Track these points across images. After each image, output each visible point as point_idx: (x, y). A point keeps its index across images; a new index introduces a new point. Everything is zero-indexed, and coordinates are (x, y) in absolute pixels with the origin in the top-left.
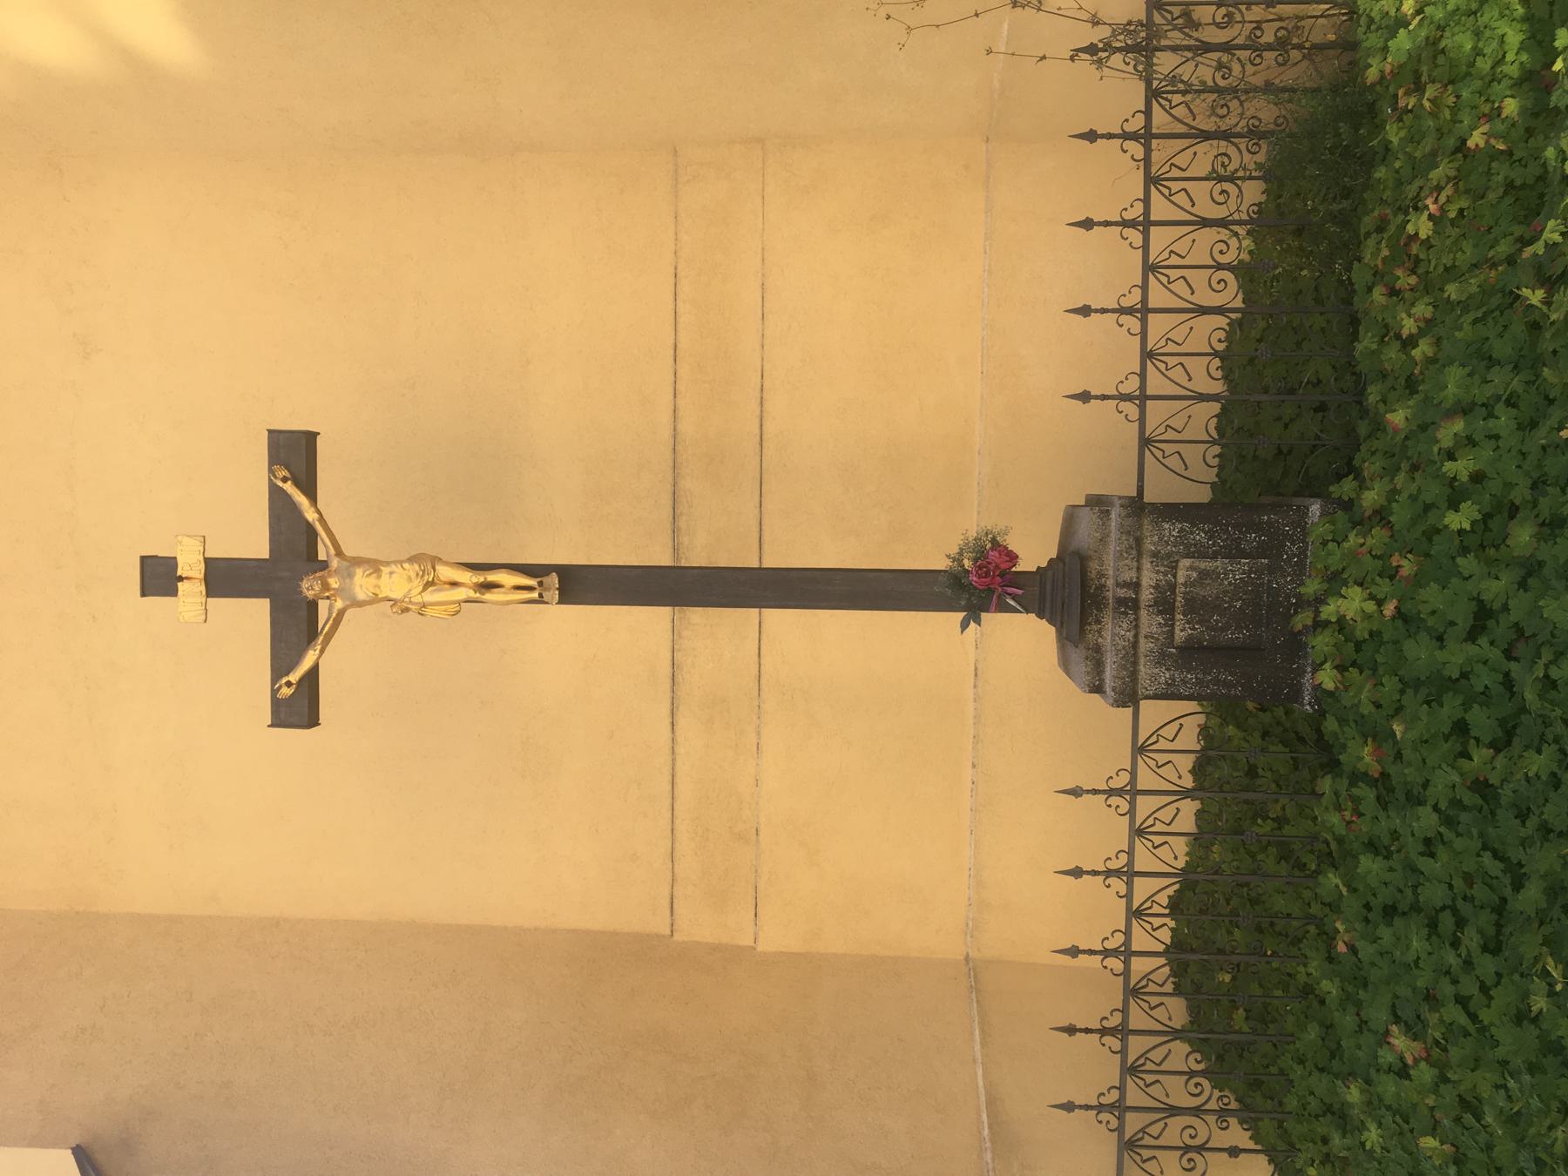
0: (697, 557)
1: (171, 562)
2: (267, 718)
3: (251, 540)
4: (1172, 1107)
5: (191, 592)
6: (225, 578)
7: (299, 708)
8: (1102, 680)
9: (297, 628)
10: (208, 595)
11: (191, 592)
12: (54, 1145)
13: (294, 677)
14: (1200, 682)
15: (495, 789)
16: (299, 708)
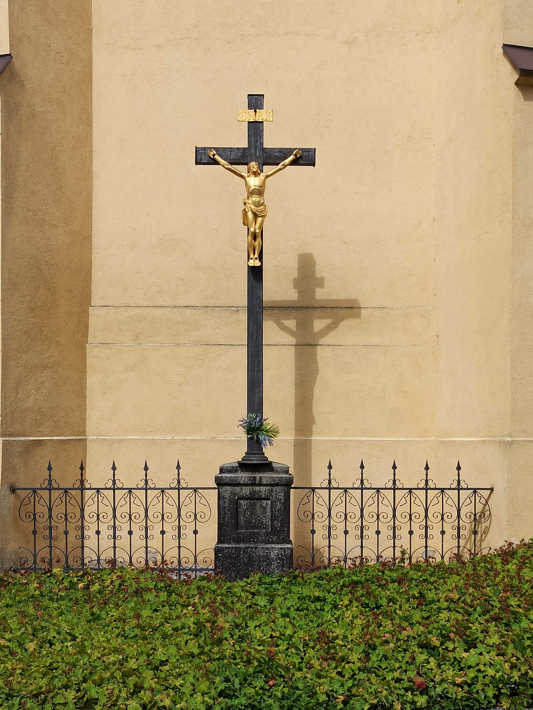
0: (244, 301)
1: (261, 107)
2: (358, 320)
3: (271, 140)
4: (83, 510)
5: (251, 116)
6: (255, 129)
7: (204, 157)
8: (224, 473)
9: (237, 158)
10: (249, 122)
11: (251, 116)
12: (11, 46)
13: (217, 157)
14: (225, 508)
15: (152, 222)
16: (204, 157)
